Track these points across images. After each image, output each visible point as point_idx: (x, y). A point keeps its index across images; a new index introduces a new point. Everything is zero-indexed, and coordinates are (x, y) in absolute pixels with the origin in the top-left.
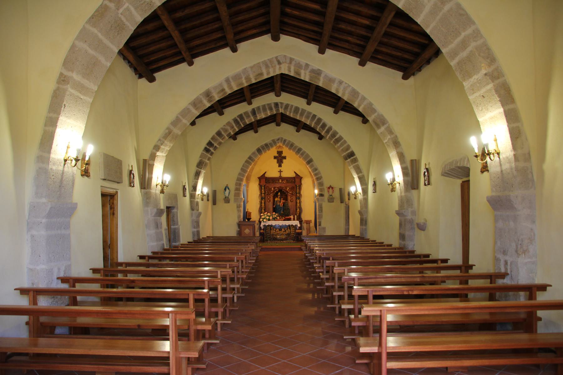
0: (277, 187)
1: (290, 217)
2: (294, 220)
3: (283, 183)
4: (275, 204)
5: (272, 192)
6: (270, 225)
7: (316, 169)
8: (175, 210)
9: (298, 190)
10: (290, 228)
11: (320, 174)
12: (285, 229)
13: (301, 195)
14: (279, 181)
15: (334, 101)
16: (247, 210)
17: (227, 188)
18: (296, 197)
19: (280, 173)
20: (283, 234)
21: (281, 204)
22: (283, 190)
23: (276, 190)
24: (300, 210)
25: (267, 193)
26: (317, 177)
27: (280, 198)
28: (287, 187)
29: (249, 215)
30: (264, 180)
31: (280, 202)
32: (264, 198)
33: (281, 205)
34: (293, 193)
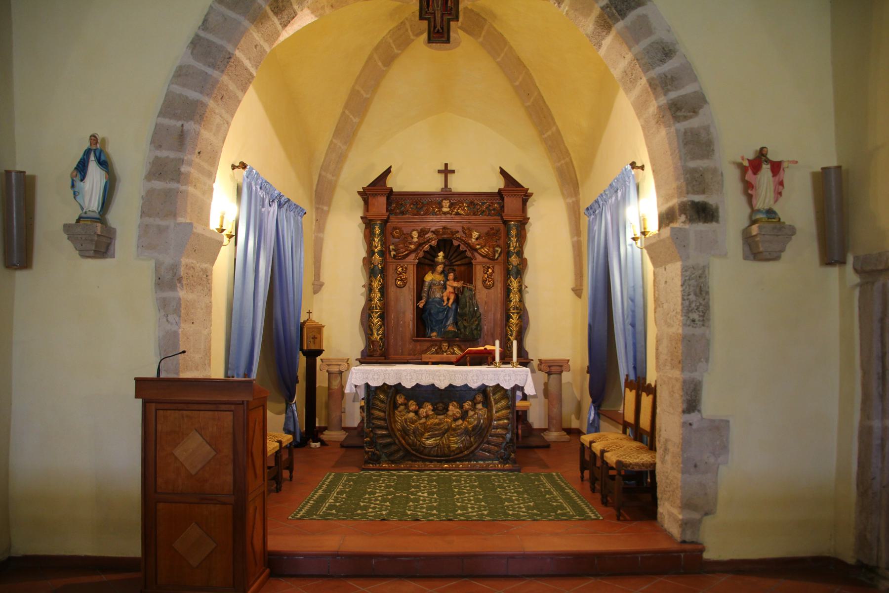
0: (433, 229)
1: (489, 347)
2: (506, 359)
3: (457, 214)
4: (424, 295)
5: (412, 247)
6: (390, 387)
7: (666, 52)
9: (514, 239)
10: (487, 403)
11: (695, 79)
12: (461, 407)
13: (526, 259)
16: (303, 318)
17: (92, 158)
19: (443, 175)
20: (454, 430)
21: (448, 297)
22: (456, 243)
25: (393, 253)
26: (673, 95)
27: (444, 273)
29: (314, 338)
31: (445, 287)
32: (383, 271)
33: (448, 299)
34: (495, 252)
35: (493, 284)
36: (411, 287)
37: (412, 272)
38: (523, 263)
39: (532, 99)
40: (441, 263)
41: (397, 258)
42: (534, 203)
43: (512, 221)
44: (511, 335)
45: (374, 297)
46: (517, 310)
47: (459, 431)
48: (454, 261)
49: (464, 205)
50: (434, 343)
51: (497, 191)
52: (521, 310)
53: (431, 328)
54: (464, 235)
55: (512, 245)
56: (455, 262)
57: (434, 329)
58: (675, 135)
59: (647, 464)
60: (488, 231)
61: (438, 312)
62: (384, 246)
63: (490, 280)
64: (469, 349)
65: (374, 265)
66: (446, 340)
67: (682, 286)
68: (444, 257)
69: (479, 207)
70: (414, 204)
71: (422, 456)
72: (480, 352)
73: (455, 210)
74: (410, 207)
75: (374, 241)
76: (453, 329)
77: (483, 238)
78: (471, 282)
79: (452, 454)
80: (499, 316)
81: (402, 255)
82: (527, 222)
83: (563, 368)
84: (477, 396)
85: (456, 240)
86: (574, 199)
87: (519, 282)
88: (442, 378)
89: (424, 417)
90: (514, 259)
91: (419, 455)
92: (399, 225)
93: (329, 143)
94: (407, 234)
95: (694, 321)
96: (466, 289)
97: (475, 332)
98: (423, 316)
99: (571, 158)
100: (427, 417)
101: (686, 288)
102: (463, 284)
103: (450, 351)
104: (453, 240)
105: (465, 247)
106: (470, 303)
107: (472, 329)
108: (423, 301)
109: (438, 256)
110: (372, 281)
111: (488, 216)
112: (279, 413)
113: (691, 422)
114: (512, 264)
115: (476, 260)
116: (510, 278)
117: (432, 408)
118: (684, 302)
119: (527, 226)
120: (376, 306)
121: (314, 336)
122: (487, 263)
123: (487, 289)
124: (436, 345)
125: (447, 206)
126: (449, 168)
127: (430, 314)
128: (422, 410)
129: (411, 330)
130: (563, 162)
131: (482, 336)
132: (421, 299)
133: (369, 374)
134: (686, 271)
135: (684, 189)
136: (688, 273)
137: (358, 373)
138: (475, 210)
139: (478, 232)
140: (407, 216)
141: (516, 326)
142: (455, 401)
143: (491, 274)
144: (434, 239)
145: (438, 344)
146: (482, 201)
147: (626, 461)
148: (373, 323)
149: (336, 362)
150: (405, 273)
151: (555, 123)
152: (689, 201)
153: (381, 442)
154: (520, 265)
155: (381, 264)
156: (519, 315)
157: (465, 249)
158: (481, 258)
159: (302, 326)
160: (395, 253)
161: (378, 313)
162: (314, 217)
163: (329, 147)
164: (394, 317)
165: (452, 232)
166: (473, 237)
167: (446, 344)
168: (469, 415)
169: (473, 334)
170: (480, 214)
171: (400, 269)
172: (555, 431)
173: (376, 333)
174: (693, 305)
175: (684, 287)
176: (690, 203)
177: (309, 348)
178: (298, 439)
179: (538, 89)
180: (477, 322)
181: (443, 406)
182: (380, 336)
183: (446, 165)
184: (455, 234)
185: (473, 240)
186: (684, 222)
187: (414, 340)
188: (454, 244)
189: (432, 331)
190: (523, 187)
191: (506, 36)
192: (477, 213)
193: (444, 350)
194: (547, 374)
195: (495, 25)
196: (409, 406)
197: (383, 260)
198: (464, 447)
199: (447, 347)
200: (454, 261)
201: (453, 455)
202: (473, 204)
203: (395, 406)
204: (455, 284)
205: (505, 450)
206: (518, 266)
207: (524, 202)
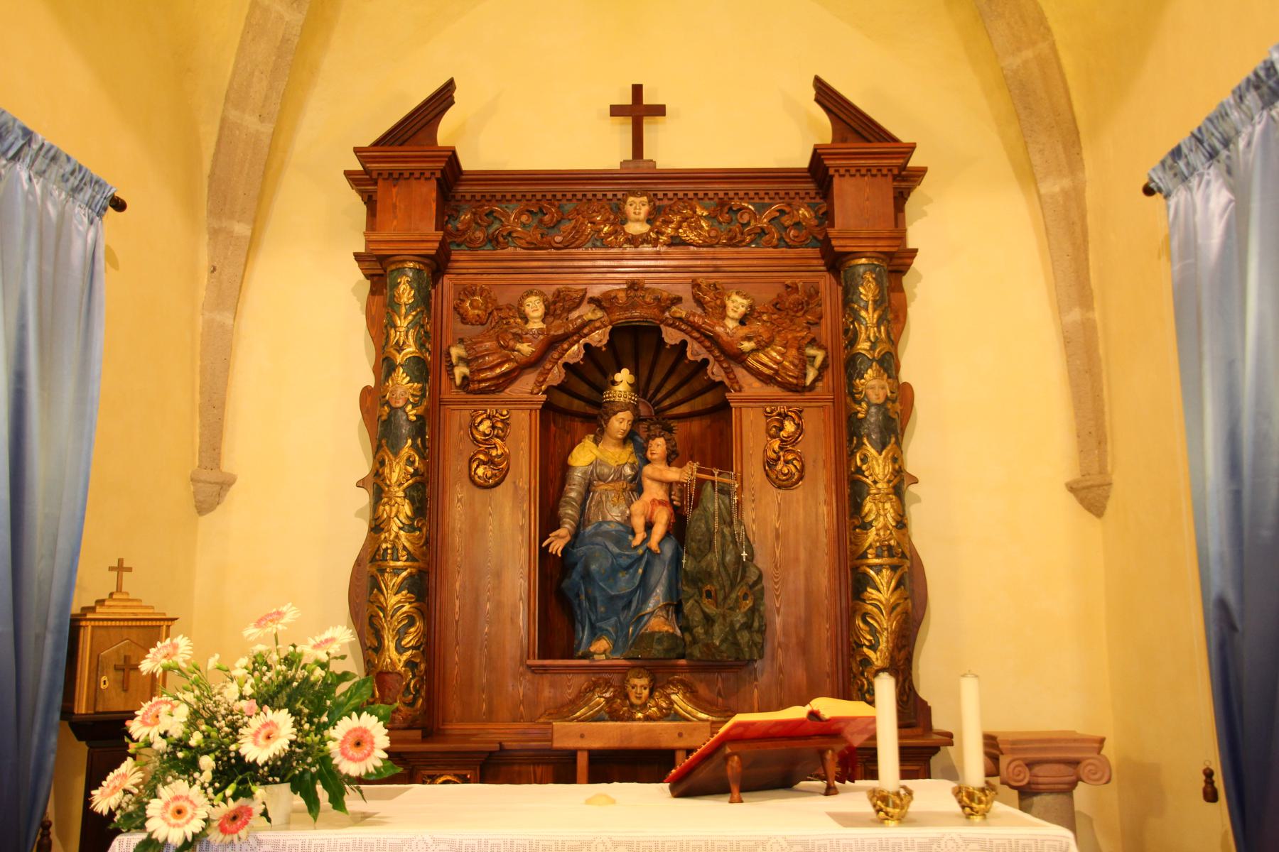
0: (595, 291)
4: (569, 512)
9: (869, 316)
14: (620, 219)
19: (628, 122)
22: (671, 336)
23: (579, 331)
25: (460, 371)
28: (720, 293)
30: (429, 191)
31: (637, 486)
33: (649, 526)
34: (805, 361)
35: (802, 471)
36: (523, 483)
38: (903, 395)
40: (625, 407)
42: (925, 208)
44: (873, 647)
45: (389, 517)
48: (667, 403)
49: (699, 212)
50: (600, 676)
51: (801, 160)
52: (903, 555)
53: (593, 626)
54: (699, 311)
55: (863, 336)
56: (672, 406)
57: (602, 630)
60: (779, 296)
61: (614, 571)
63: (790, 457)
64: (740, 718)
65: (390, 406)
66: (642, 667)
68: (635, 387)
69: (746, 218)
72: (790, 731)
73: (669, 230)
75: (395, 326)
76: (666, 628)
77: (765, 317)
78: (724, 462)
81: (489, 374)
83: (1084, 770)
85: (670, 325)
86: (1066, 183)
87: (895, 460)
90: (873, 383)
92: (483, 281)
94: (509, 307)
96: (709, 487)
97: (744, 637)
98: (566, 584)
102: (699, 471)
103: (657, 705)
104: (662, 326)
105: (704, 350)
106: (723, 536)
107: (732, 625)
109: (614, 383)
110: (382, 463)
111: (775, 247)
115: (740, 391)
119: (907, 280)
120: (394, 548)
122: (780, 400)
123: (779, 487)
124: (608, 684)
125: (642, 216)
126: (647, 100)
127: (587, 576)
129: (523, 632)
130: (1028, 54)
131: (768, 650)
132: (558, 527)
139: (745, 297)
140: (510, 250)
141: (890, 613)
144: (598, 324)
145: (616, 678)
148: (383, 609)
154: (894, 402)
155: (415, 406)
156: (899, 573)
157: (704, 354)
158: (757, 384)
159: (75, 626)
160: (466, 371)
161: (404, 574)
162: (204, 261)
163: (248, 24)
164: (463, 586)
165: (658, 300)
166: (730, 313)
167: (644, 681)
169: (736, 643)
170: (752, 241)
171: (485, 427)
177: (100, 709)
182: (409, 653)
183: (637, 90)
184: (668, 308)
185: (731, 324)
187: (529, 667)
188: (666, 340)
189: (595, 634)
190: (895, 140)
192: (739, 237)
193: (634, 700)
197: (423, 389)
199: (646, 692)
200: (667, 403)
202: (726, 209)
204: (673, 474)
206: (889, 406)
207: (901, 198)
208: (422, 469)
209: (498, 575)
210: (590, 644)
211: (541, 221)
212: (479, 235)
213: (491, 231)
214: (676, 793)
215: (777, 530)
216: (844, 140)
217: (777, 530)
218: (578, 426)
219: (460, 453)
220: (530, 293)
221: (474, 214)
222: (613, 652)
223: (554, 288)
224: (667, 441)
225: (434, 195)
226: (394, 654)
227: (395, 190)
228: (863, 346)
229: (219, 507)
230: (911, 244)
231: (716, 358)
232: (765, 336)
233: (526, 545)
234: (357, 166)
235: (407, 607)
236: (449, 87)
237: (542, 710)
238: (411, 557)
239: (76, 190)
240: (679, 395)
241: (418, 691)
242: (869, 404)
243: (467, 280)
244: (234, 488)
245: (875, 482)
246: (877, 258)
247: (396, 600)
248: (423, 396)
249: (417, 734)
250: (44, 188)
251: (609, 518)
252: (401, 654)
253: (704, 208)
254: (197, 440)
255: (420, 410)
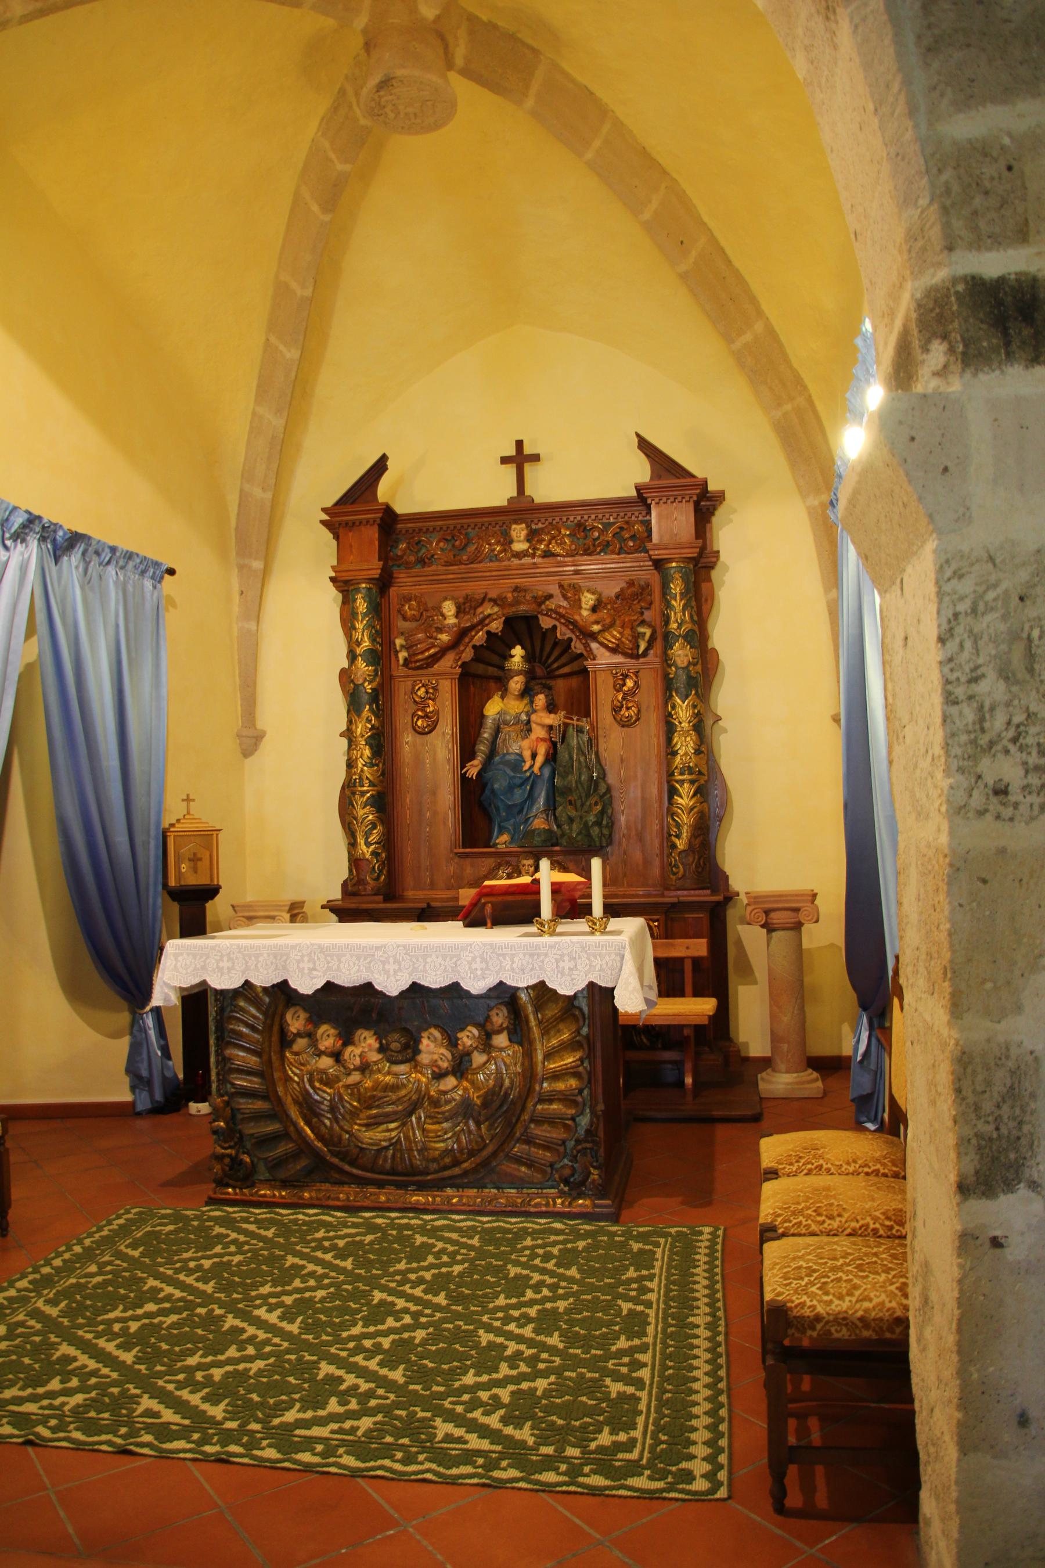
4: (482, 748)
8: (979, 808)
9: (677, 604)
10: (518, 1030)
12: (452, 1042)
15: (814, 1403)
18: (666, 676)
20: (435, 1103)
22: (546, 623)
24: (701, 792)
25: (403, 655)
28: (577, 589)
33: (534, 756)
34: (637, 637)
37: (448, 696)
39: (694, 253)
40: (519, 673)
41: (413, 665)
43: (671, 560)
44: (678, 836)
45: (357, 759)
46: (689, 774)
47: (448, 1107)
48: (555, 665)
49: (563, 532)
52: (700, 773)
54: (565, 604)
56: (559, 668)
57: (505, 828)
58: (885, 17)
59: (881, 1319)
60: (622, 589)
61: (511, 788)
62: (379, 640)
67: (942, 640)
68: (528, 658)
70: (446, 540)
71: (355, 1171)
74: (435, 546)
75: (355, 629)
79: (434, 1166)
80: (654, 790)
81: (420, 657)
82: (715, 563)
83: (802, 917)
84: (493, 1013)
85: (546, 615)
88: (391, 967)
89: (356, 1069)
91: (347, 1168)
92: (415, 591)
93: (249, 417)
95: (1001, 791)
97: (595, 831)
99: (810, 396)
100: (364, 1068)
101: (961, 646)
102: (566, 718)
104: (540, 616)
106: (580, 762)
108: (475, 762)
111: (619, 554)
112: (115, 1035)
113: (998, 1233)
114: (675, 664)
115: (594, 659)
116: (671, 696)
117: (377, 1045)
118: (954, 710)
119: (714, 574)
120: (360, 778)
121: (195, 854)
123: (623, 726)
125: (522, 538)
128: (350, 1049)
129: (451, 831)
130: (788, 407)
131: (616, 837)
133: (208, 956)
134: (959, 575)
135: (935, 233)
136: (966, 586)
137: (182, 954)
138: (589, 542)
140: (434, 567)
141: (689, 813)
142: (436, 1027)
143: (632, 693)
144: (495, 617)
145: (513, 860)
146: (605, 521)
147: (802, 1305)
148: (356, 819)
149: (266, 911)
150: (433, 700)
151: (760, 313)
152: (955, 281)
153: (252, 1131)
154: (695, 665)
156: (696, 785)
158: (607, 654)
162: (236, 588)
165: (535, 598)
166: (584, 606)
168: (474, 1066)
169: (589, 835)
171: (421, 692)
172: (788, 1072)
173: (362, 842)
174: (998, 722)
175: (952, 646)
176: (960, 288)
177: (183, 883)
178: (159, 1096)
179: (709, 229)
180: (599, 808)
181: (403, 1040)
183: (519, 444)
184: (543, 602)
185: (585, 613)
186: (942, 373)
191: (600, 93)
194: (765, 930)
195: (565, 66)
196: (317, 1040)
197: (376, 671)
198: (461, 1150)
200: (555, 665)
201: (436, 1172)
203: (285, 1041)
205: (574, 1159)
208: (377, 724)
209: (434, 793)
210: (497, 838)
211: (453, 546)
212: (412, 559)
213: (420, 554)
214: (467, 922)
215: (622, 757)
216: (660, 477)
217: (622, 757)
218: (492, 685)
219: (406, 711)
220: (445, 599)
221: (408, 543)
222: (510, 843)
223: (464, 593)
224: (546, 696)
225: (377, 535)
226: (364, 848)
227: (350, 534)
228: (674, 626)
229: (257, 753)
230: (715, 549)
231: (577, 637)
232: (608, 621)
233: (451, 771)
234: (326, 517)
235: (371, 817)
236: (384, 458)
237: (466, 882)
238: (372, 784)
239: (143, 573)
240: (563, 660)
241: (381, 871)
242: (677, 668)
243: (405, 591)
244: (265, 740)
245: (680, 723)
246: (683, 562)
247: (365, 814)
248: (376, 675)
249: (381, 898)
250: (125, 575)
251: (511, 751)
252: (368, 847)
253: (567, 528)
254: (239, 708)
255: (374, 685)
